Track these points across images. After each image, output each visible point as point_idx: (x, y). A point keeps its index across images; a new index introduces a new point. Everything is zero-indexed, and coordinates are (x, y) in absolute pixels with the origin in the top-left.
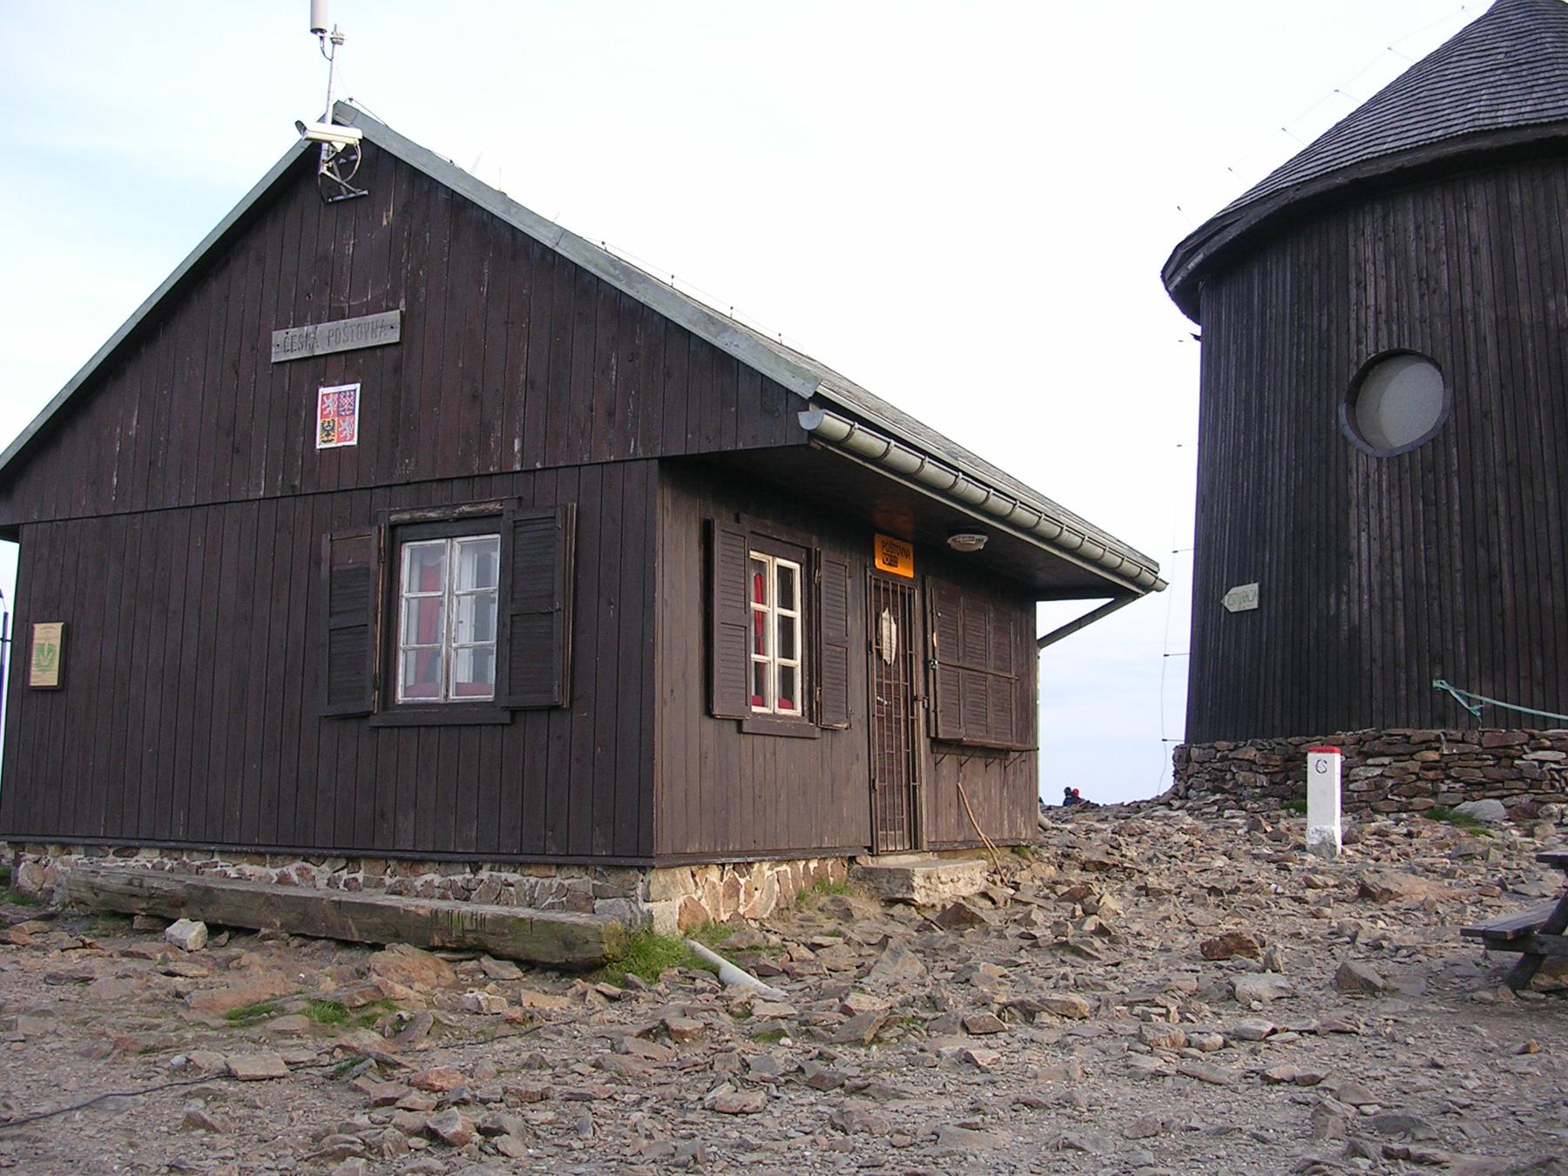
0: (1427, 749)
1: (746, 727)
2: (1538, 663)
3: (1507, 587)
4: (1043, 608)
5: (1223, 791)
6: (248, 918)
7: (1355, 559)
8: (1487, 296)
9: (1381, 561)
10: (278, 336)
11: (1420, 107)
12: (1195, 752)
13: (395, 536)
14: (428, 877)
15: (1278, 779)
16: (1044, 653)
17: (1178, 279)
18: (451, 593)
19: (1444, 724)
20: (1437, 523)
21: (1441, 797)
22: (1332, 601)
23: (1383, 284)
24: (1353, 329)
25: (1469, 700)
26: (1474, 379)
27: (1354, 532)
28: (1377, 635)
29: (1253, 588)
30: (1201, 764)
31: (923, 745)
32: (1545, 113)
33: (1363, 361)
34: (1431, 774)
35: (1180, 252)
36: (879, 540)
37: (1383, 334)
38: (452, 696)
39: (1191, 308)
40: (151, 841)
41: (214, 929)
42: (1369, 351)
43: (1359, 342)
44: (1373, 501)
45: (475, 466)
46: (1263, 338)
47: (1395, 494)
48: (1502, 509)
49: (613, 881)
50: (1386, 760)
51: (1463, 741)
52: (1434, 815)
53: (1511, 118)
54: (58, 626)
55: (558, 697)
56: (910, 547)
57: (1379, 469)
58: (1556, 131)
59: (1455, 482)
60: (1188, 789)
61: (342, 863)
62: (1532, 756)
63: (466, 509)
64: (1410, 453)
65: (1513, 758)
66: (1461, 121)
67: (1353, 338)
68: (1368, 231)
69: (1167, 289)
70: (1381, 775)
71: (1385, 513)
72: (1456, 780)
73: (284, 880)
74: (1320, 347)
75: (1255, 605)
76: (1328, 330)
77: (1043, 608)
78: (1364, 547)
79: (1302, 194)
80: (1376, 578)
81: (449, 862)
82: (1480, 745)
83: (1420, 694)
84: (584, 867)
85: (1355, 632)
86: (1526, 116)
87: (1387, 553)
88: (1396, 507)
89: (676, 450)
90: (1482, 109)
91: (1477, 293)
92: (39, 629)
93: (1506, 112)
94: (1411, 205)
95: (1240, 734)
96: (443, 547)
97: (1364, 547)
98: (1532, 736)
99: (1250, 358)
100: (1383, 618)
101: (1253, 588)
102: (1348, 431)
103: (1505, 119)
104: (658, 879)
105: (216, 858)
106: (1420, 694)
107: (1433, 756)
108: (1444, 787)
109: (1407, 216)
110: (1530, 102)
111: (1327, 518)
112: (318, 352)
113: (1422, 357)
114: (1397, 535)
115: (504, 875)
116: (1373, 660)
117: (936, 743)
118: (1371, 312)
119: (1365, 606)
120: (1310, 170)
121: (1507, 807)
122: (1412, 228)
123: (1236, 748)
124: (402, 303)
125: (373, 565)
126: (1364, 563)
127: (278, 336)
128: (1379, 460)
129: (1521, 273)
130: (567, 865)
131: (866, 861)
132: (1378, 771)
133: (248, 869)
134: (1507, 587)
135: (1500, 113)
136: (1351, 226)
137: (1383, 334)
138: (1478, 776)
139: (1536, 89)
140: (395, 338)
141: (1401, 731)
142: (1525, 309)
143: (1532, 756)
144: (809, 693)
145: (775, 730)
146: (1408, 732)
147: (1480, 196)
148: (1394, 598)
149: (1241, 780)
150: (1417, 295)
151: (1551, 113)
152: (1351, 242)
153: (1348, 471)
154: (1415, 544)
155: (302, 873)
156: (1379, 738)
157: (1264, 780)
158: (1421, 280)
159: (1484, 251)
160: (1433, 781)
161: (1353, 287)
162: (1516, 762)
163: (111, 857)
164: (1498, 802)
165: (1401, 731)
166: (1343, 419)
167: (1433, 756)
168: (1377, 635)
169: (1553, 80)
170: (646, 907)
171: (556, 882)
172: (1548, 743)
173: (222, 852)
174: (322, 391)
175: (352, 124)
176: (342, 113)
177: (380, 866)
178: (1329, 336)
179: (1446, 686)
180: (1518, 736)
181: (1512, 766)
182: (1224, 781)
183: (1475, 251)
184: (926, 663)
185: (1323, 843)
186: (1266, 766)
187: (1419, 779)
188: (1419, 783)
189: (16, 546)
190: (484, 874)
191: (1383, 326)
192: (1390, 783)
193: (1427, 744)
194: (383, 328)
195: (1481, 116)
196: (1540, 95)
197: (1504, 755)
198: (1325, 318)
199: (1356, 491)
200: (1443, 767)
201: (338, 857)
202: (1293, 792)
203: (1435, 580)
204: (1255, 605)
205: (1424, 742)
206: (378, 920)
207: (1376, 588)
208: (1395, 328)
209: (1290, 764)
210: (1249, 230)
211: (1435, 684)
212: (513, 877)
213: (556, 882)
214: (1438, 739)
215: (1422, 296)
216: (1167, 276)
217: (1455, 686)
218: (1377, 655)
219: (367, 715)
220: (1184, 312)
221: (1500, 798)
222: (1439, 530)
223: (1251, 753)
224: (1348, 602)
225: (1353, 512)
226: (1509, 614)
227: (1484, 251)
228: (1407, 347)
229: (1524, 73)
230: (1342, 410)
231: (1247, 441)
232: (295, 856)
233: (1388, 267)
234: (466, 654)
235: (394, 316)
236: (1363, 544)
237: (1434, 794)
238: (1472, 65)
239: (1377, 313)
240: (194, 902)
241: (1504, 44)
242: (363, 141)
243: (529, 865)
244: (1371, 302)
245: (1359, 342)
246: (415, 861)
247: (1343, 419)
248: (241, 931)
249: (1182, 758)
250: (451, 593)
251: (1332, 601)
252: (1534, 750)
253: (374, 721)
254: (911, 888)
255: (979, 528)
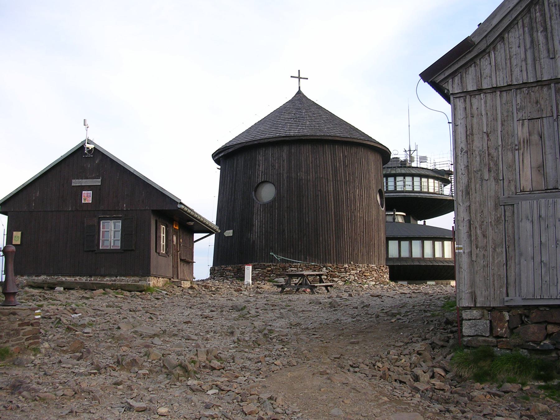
0: (269, 267)
1: (160, 254)
2: (292, 250)
3: (286, 234)
4: (195, 235)
5: (223, 277)
6: (72, 286)
7: (254, 226)
8: (286, 171)
9: (260, 227)
10: (73, 181)
11: (274, 126)
12: (216, 268)
13: (100, 219)
14: (107, 279)
15: (236, 274)
16: (195, 244)
17: (217, 158)
18: (111, 230)
19: (272, 262)
20: (272, 219)
21: (271, 277)
22: (249, 234)
23: (264, 166)
24: (257, 175)
25: (277, 257)
26: (282, 189)
27: (255, 220)
28: (258, 242)
29: (232, 231)
30: (218, 271)
31: (179, 260)
32: (300, 133)
33: (258, 182)
34: (269, 273)
35: (217, 152)
36: (174, 222)
37: (263, 177)
38: (111, 248)
39: (217, 162)
40: (44, 274)
41: (64, 289)
42: (260, 180)
43: (258, 178)
44: (259, 213)
45: (117, 208)
46: (236, 174)
47: (264, 212)
48: (286, 217)
49: (143, 278)
50: (260, 270)
51: (276, 266)
52: (269, 281)
53: (293, 133)
54: (20, 233)
55: (133, 248)
56: (178, 223)
57: (261, 206)
58: (302, 138)
59: (277, 211)
60: (214, 277)
61: (88, 277)
62: (290, 269)
63: (114, 216)
64: (267, 204)
65: (286, 269)
66: (283, 132)
67: (256, 177)
68: (261, 154)
69: (213, 159)
70: (259, 273)
71: (261, 216)
72: (274, 274)
73: (75, 280)
74: (249, 179)
75: (232, 235)
76: (251, 175)
77: (195, 235)
78: (257, 224)
79: (247, 144)
80: (259, 231)
81: (111, 276)
82: (279, 266)
83: (267, 256)
84: (137, 276)
85: (254, 242)
86: (296, 133)
87: (262, 225)
88: (264, 215)
89: (155, 209)
90: (288, 130)
91: (283, 170)
92: (15, 233)
93: (292, 132)
94: (271, 149)
95: (227, 264)
96: (109, 222)
97: (257, 224)
98: (290, 265)
99: (233, 178)
100: (260, 239)
101: (232, 231)
102: (254, 198)
103: (292, 133)
104: (150, 278)
105: (60, 277)
106: (267, 256)
107: (270, 269)
108: (272, 275)
109: (270, 151)
110: (298, 130)
111: (249, 216)
112: (83, 185)
113: (271, 183)
114: (264, 221)
115: (122, 278)
116: (257, 248)
117: (181, 260)
118: (261, 172)
119: (256, 236)
120: (249, 138)
121: (285, 280)
122: (271, 154)
123: (226, 267)
124: (101, 178)
125: (96, 224)
126: (256, 227)
127: (73, 181)
128: (261, 205)
129: (293, 167)
130: (134, 276)
131: (172, 280)
132: (258, 272)
133: (68, 278)
134: (286, 234)
135: (291, 132)
136: (258, 152)
137: (263, 177)
138: (279, 273)
139: (299, 126)
140: (100, 184)
141: (263, 263)
142: (293, 175)
143: (290, 269)
144: (166, 249)
145: (163, 255)
146: (265, 264)
147: (286, 149)
148: (263, 234)
149: (227, 274)
150: (271, 169)
151: (302, 133)
152: (257, 156)
153: (254, 206)
154: (268, 223)
155: (80, 279)
156: (258, 265)
157: (233, 274)
158: (272, 166)
159: (285, 161)
160: (269, 274)
161: (257, 167)
162: (287, 270)
163: (34, 277)
164: (283, 279)
165: (263, 263)
166: (253, 195)
167: (270, 269)
168: (258, 242)
169: (303, 124)
170: (149, 282)
171: (132, 279)
172: (293, 266)
173: (61, 276)
174: (83, 192)
175: (92, 144)
176: (90, 142)
177: (96, 277)
178: (251, 176)
179: (273, 254)
180: (287, 265)
181: (286, 271)
182: (223, 274)
183: (284, 161)
184: (180, 245)
185: (248, 284)
186: (233, 271)
187: (266, 274)
188: (267, 275)
189: (7, 217)
190: (118, 278)
191: (263, 175)
192: (260, 274)
193: (269, 266)
194: (97, 182)
195: (287, 132)
196: (300, 128)
197: (284, 269)
198: (250, 172)
199: (255, 211)
200: (272, 271)
201: (88, 276)
202: (239, 276)
203: (271, 231)
204: (232, 235)
205: (268, 266)
206: (100, 285)
207: (259, 232)
208: (266, 176)
209: (239, 271)
210: (235, 150)
211: (271, 253)
212: (124, 278)
213: (132, 279)
214: (271, 265)
215: (272, 169)
216: (214, 155)
217: (275, 254)
218: (258, 246)
219: (95, 251)
220: (216, 163)
221: (283, 278)
222: (273, 221)
223: (230, 268)
224: (253, 235)
225: (254, 216)
226: (286, 240)
227: (285, 161)
228: (268, 180)
229: (297, 121)
230: (253, 193)
231: (231, 198)
232: (78, 276)
233: (265, 163)
234: (113, 240)
235: (100, 180)
236: (256, 223)
237: (270, 277)
238: (287, 116)
239: (262, 172)
240: (61, 284)
241: (294, 111)
242: (94, 148)
243: (127, 276)
244: (261, 170)
245: (258, 178)
246: (104, 276)
247: (253, 195)
248: (69, 289)
249: (212, 271)
250: (111, 230)
251: (249, 234)
252: (290, 268)
253: (96, 252)
254: (181, 284)
255: (192, 221)
